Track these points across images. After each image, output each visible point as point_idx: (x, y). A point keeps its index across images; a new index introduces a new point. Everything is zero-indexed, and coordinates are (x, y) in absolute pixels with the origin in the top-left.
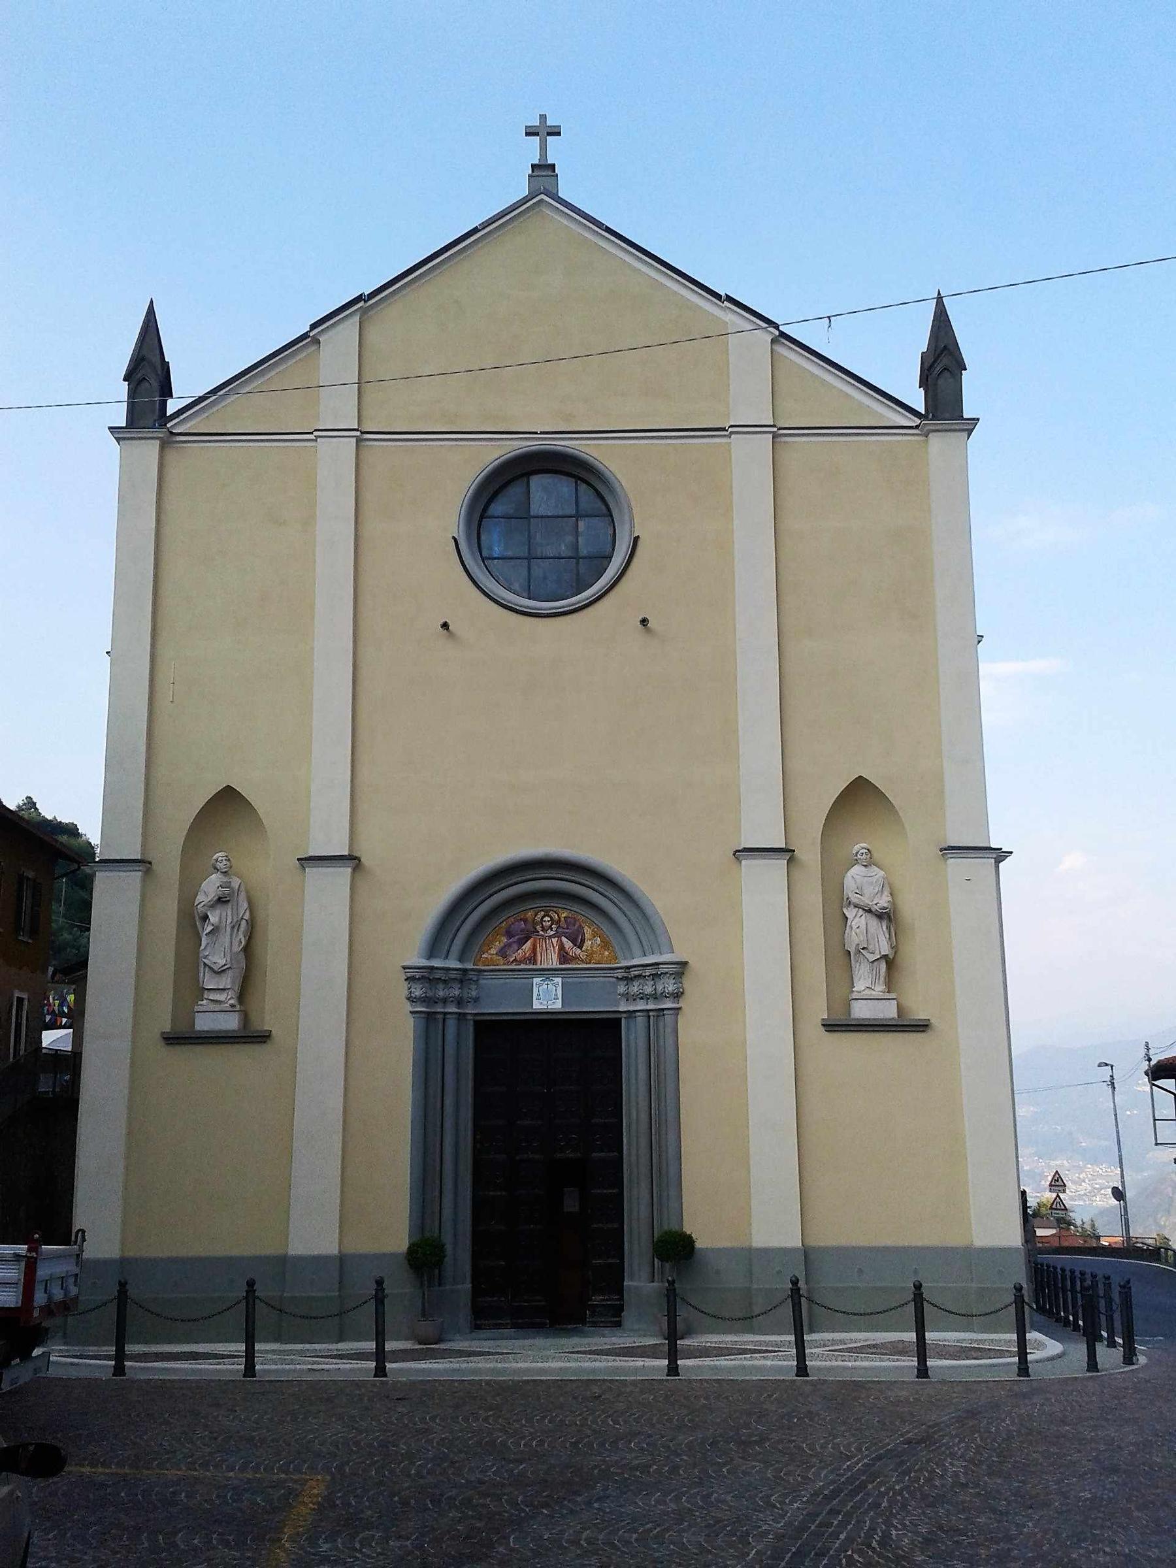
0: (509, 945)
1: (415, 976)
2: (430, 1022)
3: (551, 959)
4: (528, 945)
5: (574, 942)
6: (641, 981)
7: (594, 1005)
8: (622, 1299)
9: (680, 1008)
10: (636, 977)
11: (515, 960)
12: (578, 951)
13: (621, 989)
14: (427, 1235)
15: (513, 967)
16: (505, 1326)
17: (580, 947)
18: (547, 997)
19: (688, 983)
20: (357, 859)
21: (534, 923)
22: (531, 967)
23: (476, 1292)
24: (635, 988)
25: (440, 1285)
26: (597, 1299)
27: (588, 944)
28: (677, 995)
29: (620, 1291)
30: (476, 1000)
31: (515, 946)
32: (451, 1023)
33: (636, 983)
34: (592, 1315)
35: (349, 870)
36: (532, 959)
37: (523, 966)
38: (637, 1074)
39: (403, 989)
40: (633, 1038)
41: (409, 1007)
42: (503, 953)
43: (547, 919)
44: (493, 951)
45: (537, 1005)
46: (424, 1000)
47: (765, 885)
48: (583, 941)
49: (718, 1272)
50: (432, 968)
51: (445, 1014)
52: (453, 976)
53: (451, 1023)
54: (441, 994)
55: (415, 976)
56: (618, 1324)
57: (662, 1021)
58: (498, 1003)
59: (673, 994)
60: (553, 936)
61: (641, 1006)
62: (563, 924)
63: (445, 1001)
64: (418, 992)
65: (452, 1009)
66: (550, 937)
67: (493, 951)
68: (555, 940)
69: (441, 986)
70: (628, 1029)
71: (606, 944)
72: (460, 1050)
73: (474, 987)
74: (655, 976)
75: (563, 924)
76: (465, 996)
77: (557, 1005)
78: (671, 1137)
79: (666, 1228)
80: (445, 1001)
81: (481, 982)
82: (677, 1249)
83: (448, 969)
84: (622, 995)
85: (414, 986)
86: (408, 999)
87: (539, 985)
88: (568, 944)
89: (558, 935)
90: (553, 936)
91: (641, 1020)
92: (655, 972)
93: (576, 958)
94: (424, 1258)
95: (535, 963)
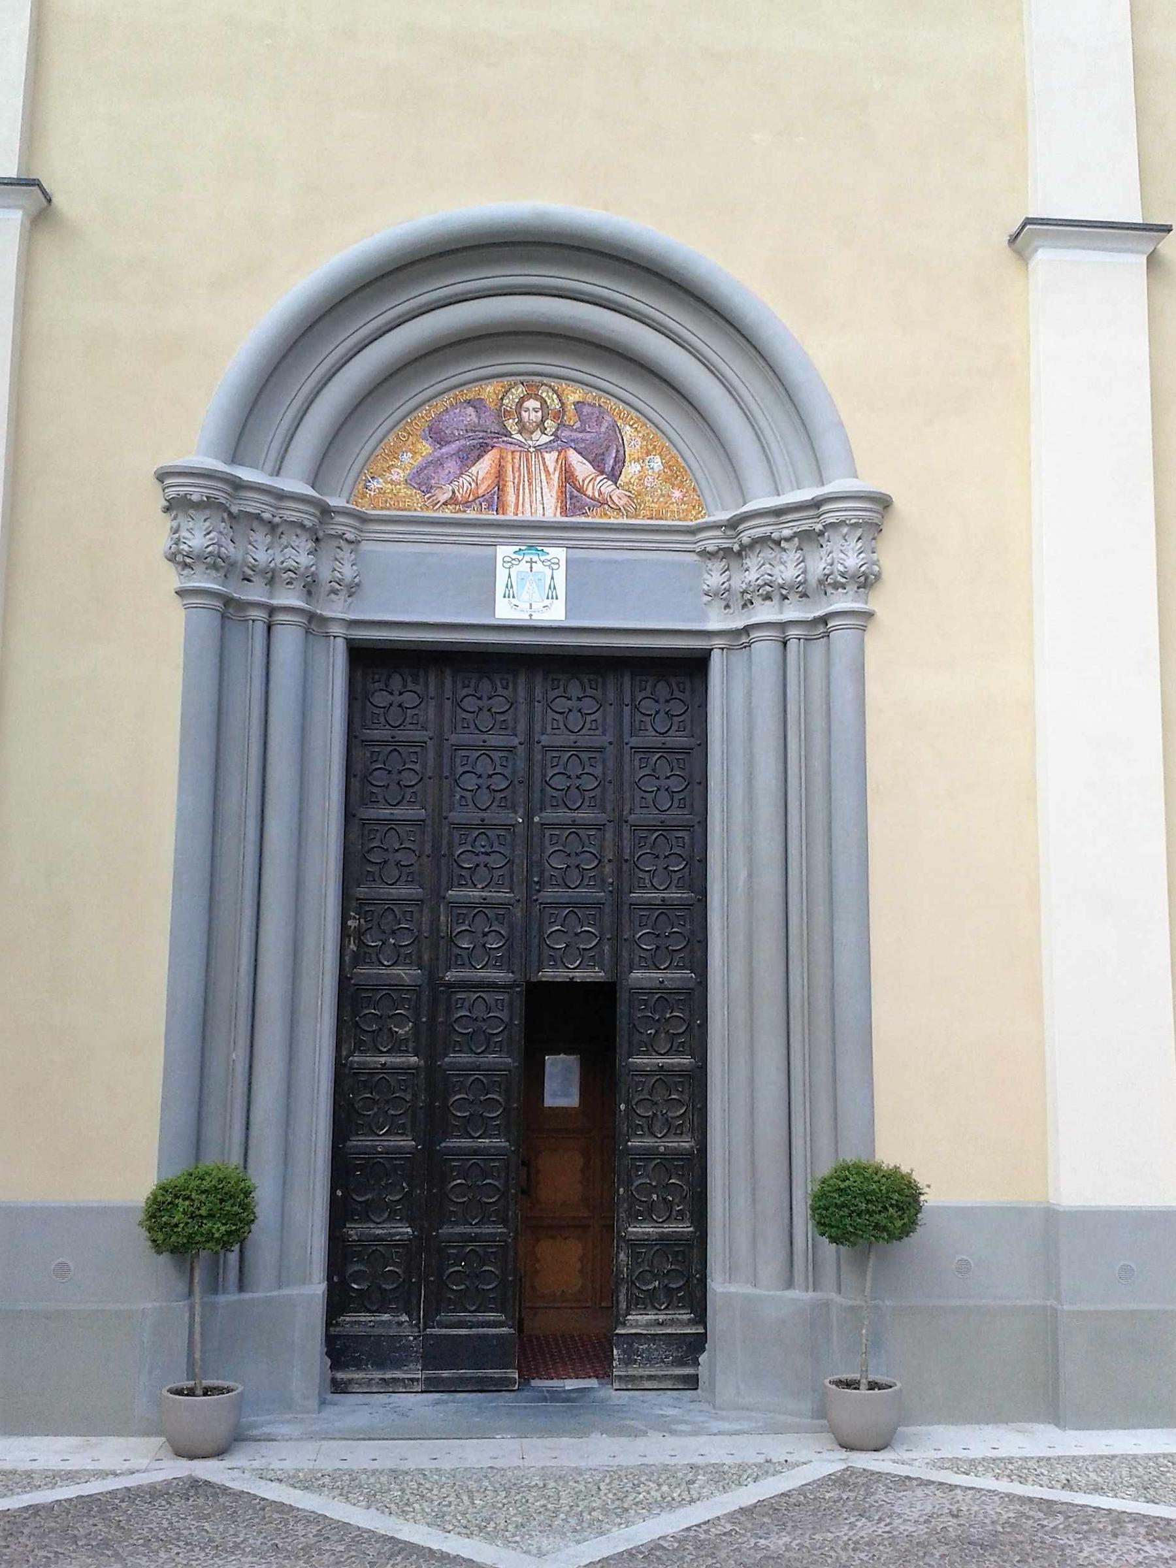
0: (438, 463)
1: (190, 496)
2: (229, 615)
3: (541, 501)
4: (484, 467)
5: (597, 463)
6: (767, 554)
7: (653, 605)
8: (701, 1317)
9: (869, 615)
10: (757, 542)
11: (453, 501)
12: (608, 487)
13: (714, 577)
14: (210, 1161)
15: (447, 513)
16: (407, 1385)
17: (614, 477)
18: (531, 594)
19: (891, 556)
20: (36, 183)
21: (501, 414)
22: (492, 516)
23: (339, 1301)
24: (753, 571)
25: (241, 1287)
26: (639, 1321)
27: (631, 470)
28: (866, 581)
29: (695, 1298)
30: (353, 589)
31: (452, 466)
32: (288, 640)
33: (752, 562)
34: (628, 1362)
35: (17, 216)
36: (496, 497)
37: (471, 514)
38: (750, 778)
39: (157, 532)
40: (736, 700)
41: (173, 579)
42: (422, 481)
43: (532, 404)
44: (398, 475)
45: (505, 612)
46: (217, 563)
47: (1090, 307)
48: (620, 462)
49: (964, 1268)
50: (238, 486)
51: (272, 610)
52: (293, 516)
53: (288, 640)
54: (262, 557)
55: (190, 496)
56: (692, 1382)
57: (822, 631)
58: (409, 596)
59: (855, 577)
60: (548, 447)
61: (765, 613)
62: (571, 417)
63: (271, 578)
64: (197, 538)
65: (289, 598)
66: (538, 449)
67: (398, 475)
68: (550, 458)
69: (260, 537)
70: (728, 672)
71: (674, 474)
72: (313, 706)
73: (346, 555)
74: (810, 538)
75: (571, 417)
76: (325, 574)
77: (556, 614)
78: (846, 929)
79: (850, 1158)
80: (271, 578)
81: (365, 546)
82: (869, 1212)
83: (281, 496)
84: (714, 594)
85: (186, 524)
86: (172, 558)
87: (510, 563)
88: (582, 469)
89: (559, 443)
90: (548, 447)
91: (764, 650)
92: (810, 525)
93: (602, 502)
94: (198, 1224)
95: (501, 507)
